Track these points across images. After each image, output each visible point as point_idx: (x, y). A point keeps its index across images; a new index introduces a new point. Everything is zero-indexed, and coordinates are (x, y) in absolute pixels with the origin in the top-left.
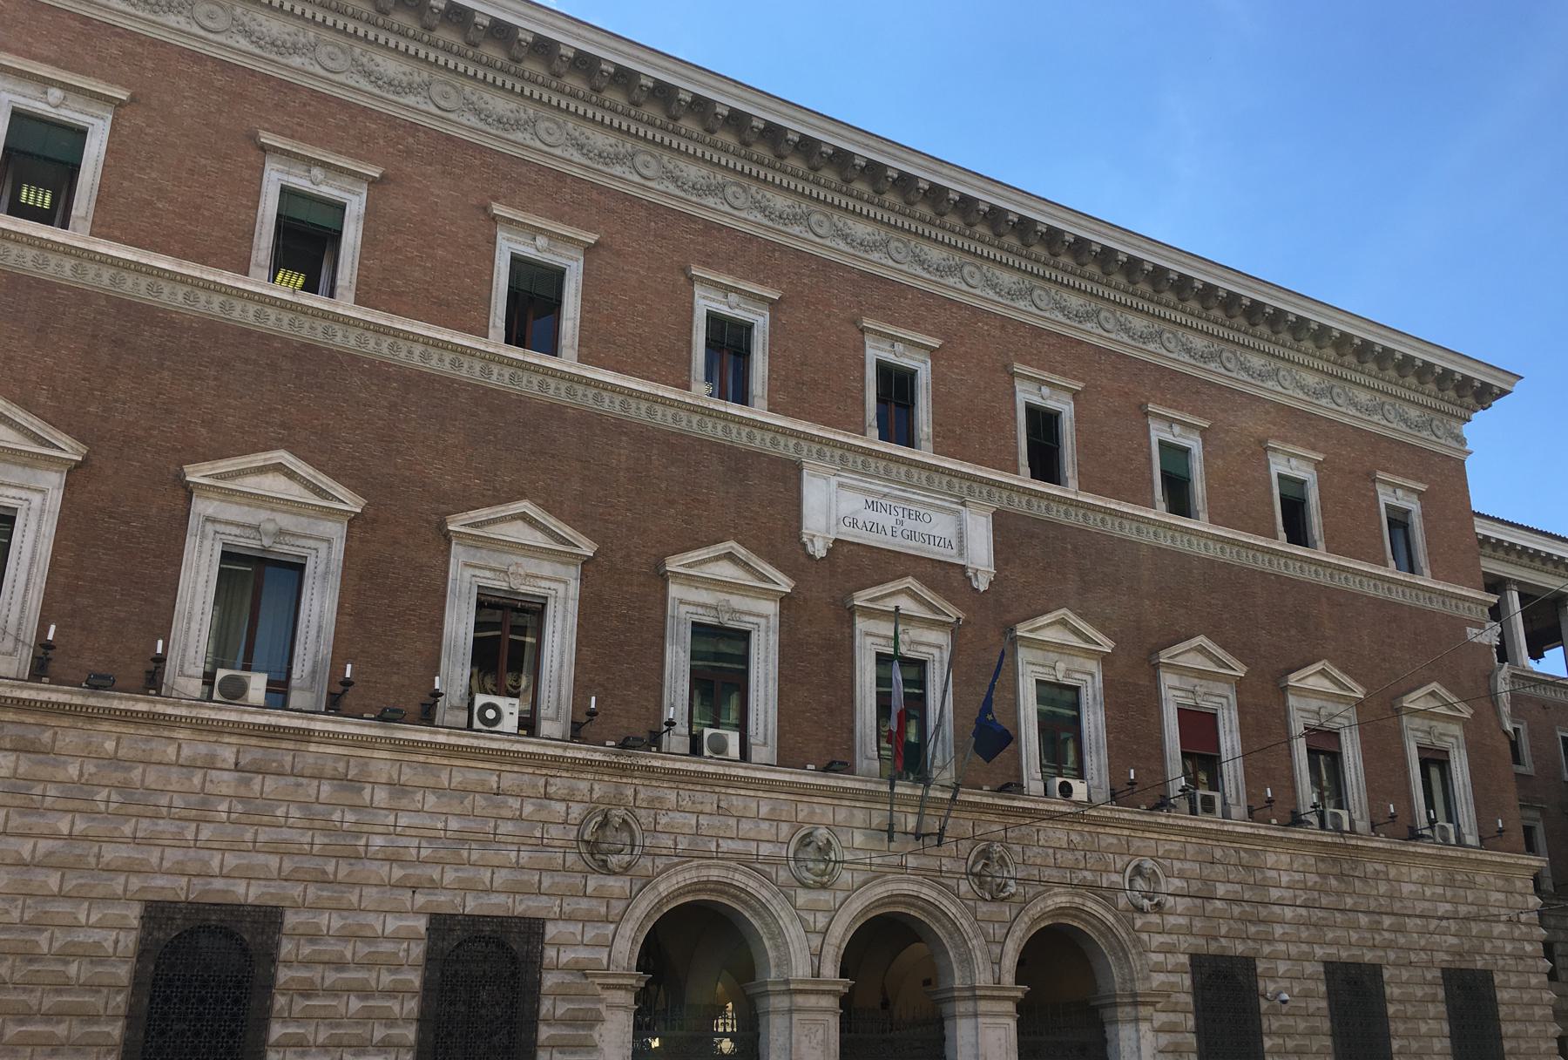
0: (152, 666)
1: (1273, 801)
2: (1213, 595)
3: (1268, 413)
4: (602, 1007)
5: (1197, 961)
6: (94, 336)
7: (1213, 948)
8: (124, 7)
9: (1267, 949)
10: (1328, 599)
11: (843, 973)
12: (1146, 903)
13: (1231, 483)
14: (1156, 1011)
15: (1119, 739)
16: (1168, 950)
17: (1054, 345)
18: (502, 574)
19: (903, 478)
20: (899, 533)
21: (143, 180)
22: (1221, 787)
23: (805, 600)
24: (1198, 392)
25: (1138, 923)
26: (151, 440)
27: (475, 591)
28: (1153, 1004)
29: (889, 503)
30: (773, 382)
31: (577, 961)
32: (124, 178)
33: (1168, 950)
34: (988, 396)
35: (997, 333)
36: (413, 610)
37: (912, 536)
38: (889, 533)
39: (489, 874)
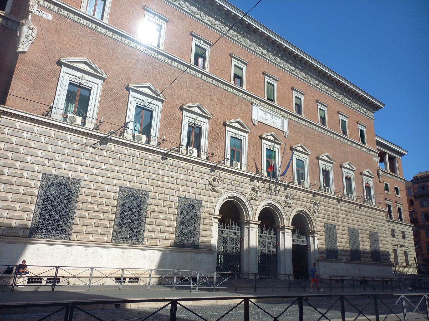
0: (49, 110)
4: (213, 222)
6: (109, 48)
7: (329, 222)
11: (220, 213)
12: (317, 211)
16: (320, 222)
18: (78, 78)
19: (263, 105)
20: (271, 121)
21: (119, 12)
22: (240, 161)
24: (326, 98)
25: (315, 215)
26: (121, 76)
28: (317, 233)
30: (247, 83)
31: (208, 211)
32: (115, 11)
33: (320, 222)
36: (176, 125)
38: (269, 121)
39: (191, 189)
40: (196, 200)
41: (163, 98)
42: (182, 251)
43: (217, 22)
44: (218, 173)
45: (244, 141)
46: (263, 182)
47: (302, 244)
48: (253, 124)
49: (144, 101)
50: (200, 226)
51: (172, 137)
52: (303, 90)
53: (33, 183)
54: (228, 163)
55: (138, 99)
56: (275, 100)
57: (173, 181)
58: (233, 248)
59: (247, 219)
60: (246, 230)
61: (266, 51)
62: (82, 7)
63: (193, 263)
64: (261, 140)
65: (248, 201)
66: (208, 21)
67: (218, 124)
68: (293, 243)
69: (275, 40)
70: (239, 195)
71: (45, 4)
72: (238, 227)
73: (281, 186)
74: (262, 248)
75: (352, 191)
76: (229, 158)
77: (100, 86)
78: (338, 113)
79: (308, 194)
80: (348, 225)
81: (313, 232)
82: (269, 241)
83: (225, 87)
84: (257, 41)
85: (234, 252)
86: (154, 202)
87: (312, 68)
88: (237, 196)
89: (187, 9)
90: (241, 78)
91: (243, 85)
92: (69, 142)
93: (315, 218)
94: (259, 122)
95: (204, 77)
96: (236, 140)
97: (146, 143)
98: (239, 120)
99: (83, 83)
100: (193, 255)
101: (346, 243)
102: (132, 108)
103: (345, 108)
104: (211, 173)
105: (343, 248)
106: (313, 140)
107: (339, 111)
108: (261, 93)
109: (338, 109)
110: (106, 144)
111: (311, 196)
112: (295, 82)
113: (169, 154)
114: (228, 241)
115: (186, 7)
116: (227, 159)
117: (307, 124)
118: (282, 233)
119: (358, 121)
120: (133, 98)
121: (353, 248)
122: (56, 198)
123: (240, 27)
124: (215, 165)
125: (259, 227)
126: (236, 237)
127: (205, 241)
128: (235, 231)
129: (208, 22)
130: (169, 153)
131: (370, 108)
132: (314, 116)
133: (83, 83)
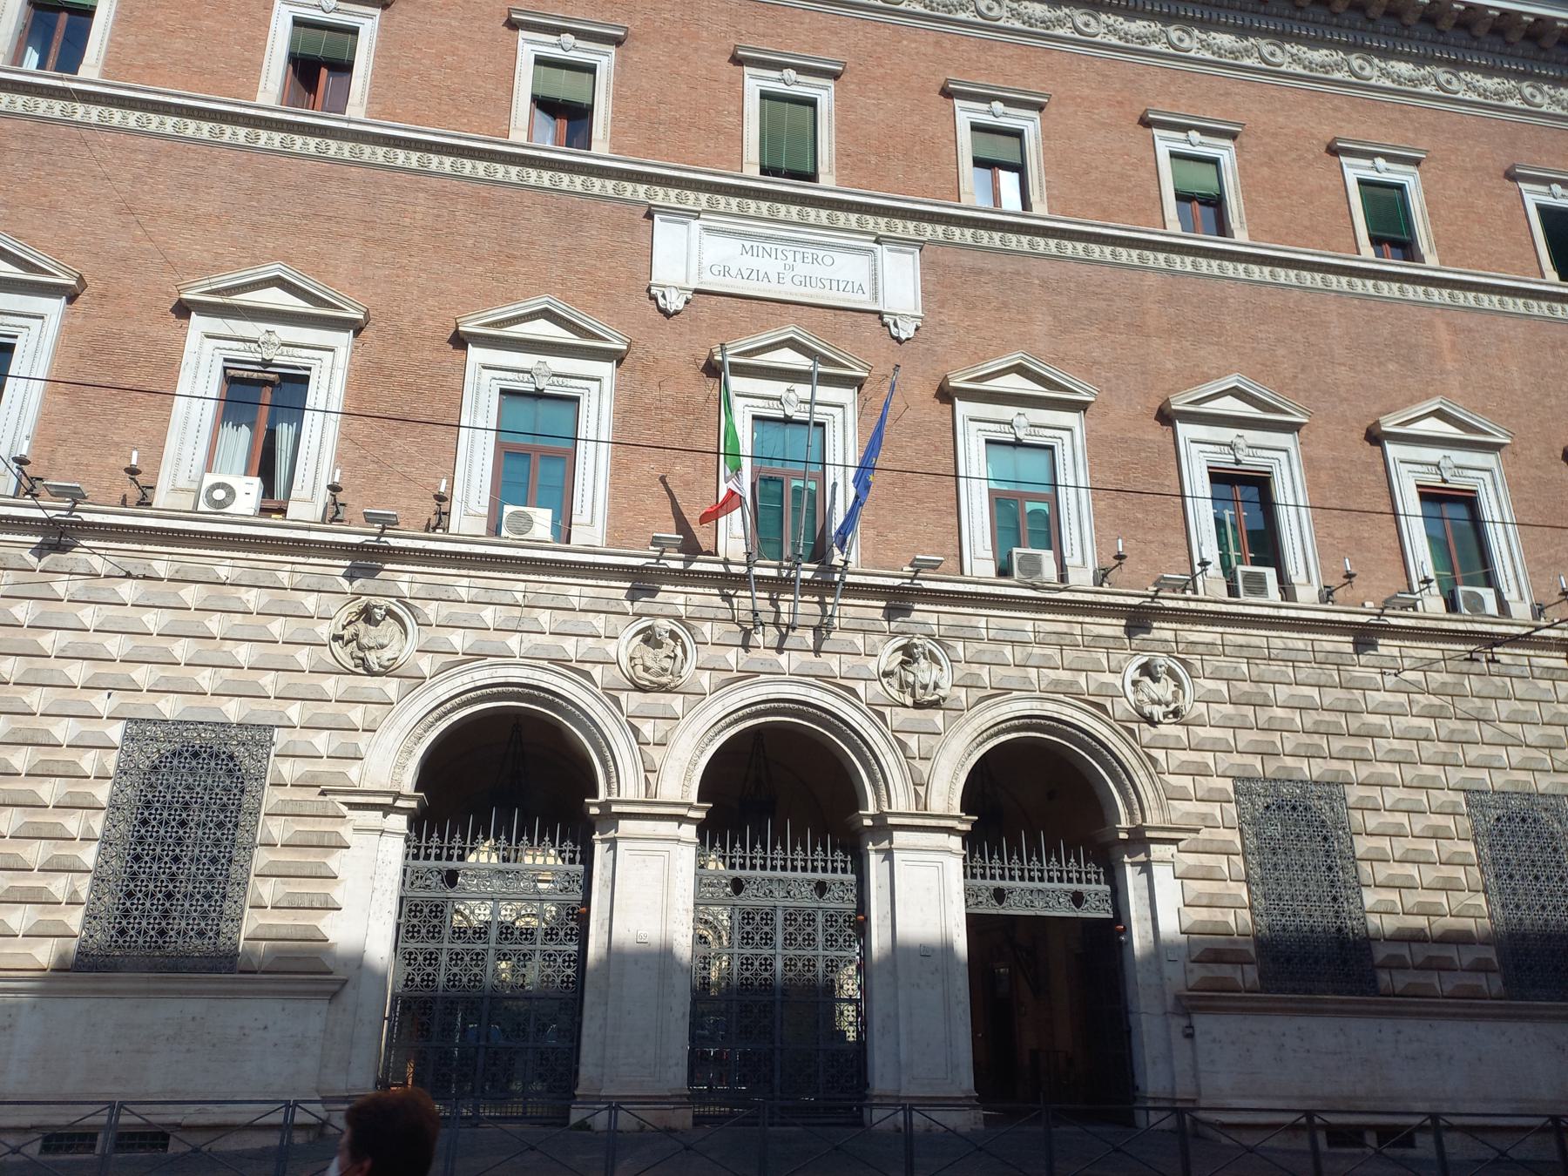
1: (1354, 575)
2: (1262, 327)
3: (1336, 109)
5: (1244, 784)
8: (880, 3)
9: (1364, 771)
10: (1448, 324)
13: (1284, 194)
14: (1179, 851)
15: (1116, 507)
17: (1011, 57)
22: (1055, 543)
23: (656, 361)
24: (1227, 94)
27: (219, 364)
29: (774, 246)
34: (916, 119)
35: (930, 50)
37: (806, 281)
40: (1316, 783)
41: (855, 370)
42: (218, 992)
43: (1334, 53)
44: (925, 616)
45: (1490, 488)
46: (720, 589)
47: (994, 912)
48: (661, 310)
49: (1010, 424)
50: (1359, 894)
51: (117, 444)
52: (1390, 140)
53: (88, 762)
54: (1433, 603)
55: (587, 379)
56: (823, 168)
57: (96, 647)
58: (431, 958)
59: (1132, 821)
60: (875, 863)
61: (1145, 23)
62: (965, 193)
63: (188, 1051)
64: (1377, 449)
65: (606, 699)
66: (1553, 107)
67: (416, 342)
68: (970, 911)
69: (1539, 19)
70: (816, 693)
71: (544, 179)
72: (1092, 867)
73: (793, 593)
74: (748, 951)
75: (1493, 565)
76: (1432, 576)
77: (608, 385)
78: (1333, 151)
79: (1088, 619)
80: (1456, 776)
81: (1139, 840)
82: (800, 910)
83: (1339, 283)
84: (1239, 17)
85: (442, 979)
86: (1372, 821)
87: (1515, 37)
88: (535, 683)
89: (1293, 66)
90: (1216, 203)
91: (1233, 226)
92: (1081, 648)
93: (1154, 752)
94: (697, 291)
95: (1339, 282)
96: (1021, 454)
97: (488, 535)
98: (1238, 381)
99: (276, 357)
100: (195, 1006)
101: (1448, 886)
102: (972, 461)
103: (1397, 115)
104: (1130, 638)
105: (1421, 922)
106: (1127, 325)
107: (1335, 139)
108: (720, 155)
109: (1327, 132)
110: (1148, 629)
111: (1345, 644)
112: (974, 56)
113: (661, 570)
114: (825, 930)
115: (1006, 14)
116: (1423, 582)
117: (1284, 276)
118: (882, 856)
119: (1329, 140)
120: (1192, 444)
121: (1531, 919)
122: (176, 810)
123: (1359, 24)
124: (1141, 600)
125: (410, 828)
126: (831, 903)
127: (283, 933)
128: (1075, 886)
129: (1112, 38)
130: (1378, 620)
131: (1547, 62)
132: (1131, 198)
133: (276, 357)
